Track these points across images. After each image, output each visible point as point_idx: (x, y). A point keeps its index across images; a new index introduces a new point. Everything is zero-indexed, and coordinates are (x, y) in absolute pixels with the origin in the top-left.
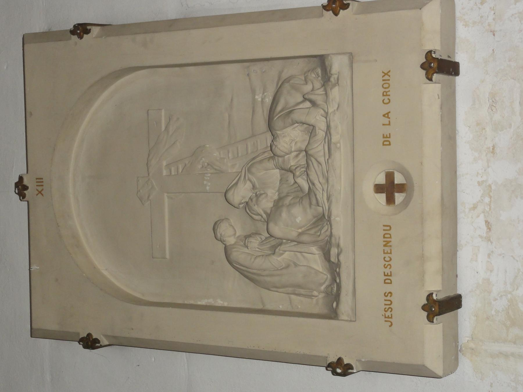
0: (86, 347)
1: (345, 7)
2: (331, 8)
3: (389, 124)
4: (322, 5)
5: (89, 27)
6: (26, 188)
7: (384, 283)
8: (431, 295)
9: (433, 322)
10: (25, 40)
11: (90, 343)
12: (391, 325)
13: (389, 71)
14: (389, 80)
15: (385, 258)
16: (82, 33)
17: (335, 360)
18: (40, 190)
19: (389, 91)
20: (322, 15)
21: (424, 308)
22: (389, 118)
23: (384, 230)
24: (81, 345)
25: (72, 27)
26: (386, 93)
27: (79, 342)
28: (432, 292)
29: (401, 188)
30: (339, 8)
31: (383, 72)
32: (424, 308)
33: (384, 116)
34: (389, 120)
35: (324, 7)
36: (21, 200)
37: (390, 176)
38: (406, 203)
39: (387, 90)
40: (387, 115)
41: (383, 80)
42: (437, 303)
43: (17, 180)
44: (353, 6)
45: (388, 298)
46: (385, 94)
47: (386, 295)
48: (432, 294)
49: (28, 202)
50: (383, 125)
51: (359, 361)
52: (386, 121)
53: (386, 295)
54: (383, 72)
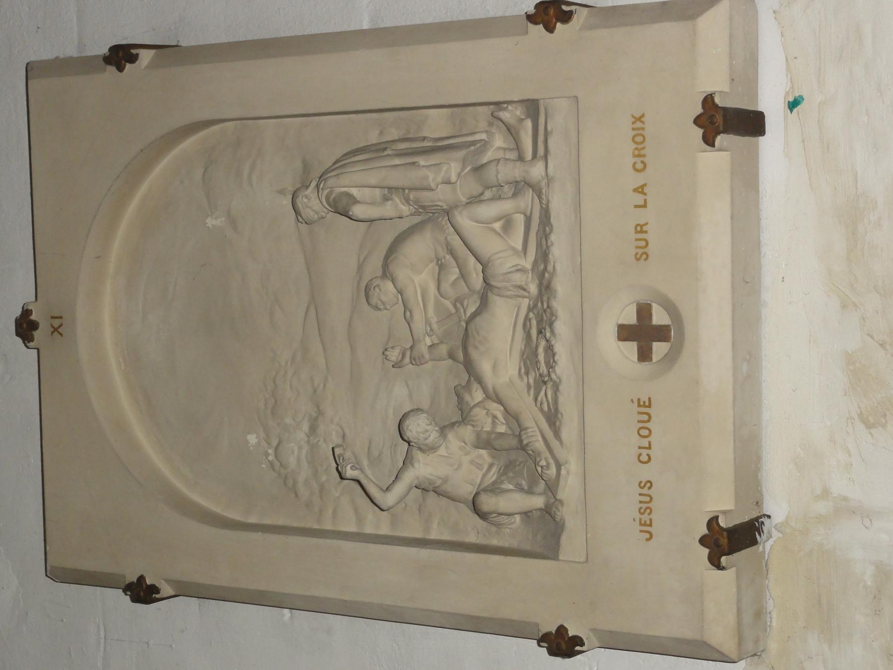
0: (136, 599)
1: (566, 17)
2: (540, 20)
3: (645, 206)
4: (526, 13)
5: (134, 51)
6: (34, 326)
7: (636, 233)
8: (715, 519)
9: (713, 145)
10: (30, 70)
11: (142, 594)
12: (647, 420)
13: (643, 115)
14: (643, 129)
15: (640, 455)
16: (123, 62)
17: (553, 629)
18: (56, 326)
19: (644, 148)
20: (526, 32)
21: (697, 121)
22: (645, 194)
23: (639, 422)
24: (128, 596)
25: (107, 51)
26: (642, 228)
27: (125, 591)
28: (787, 103)
29: (662, 333)
30: (556, 19)
31: (633, 116)
32: (697, 121)
33: (635, 190)
34: (645, 197)
35: (531, 18)
36: (28, 348)
37: (644, 311)
38: (671, 358)
39: (640, 146)
40: (640, 190)
41: (633, 129)
42: (725, 534)
43: (18, 312)
44: (580, 17)
45: (645, 491)
46: (639, 229)
47: (642, 485)
48: (717, 518)
49: (38, 349)
50: (636, 206)
51: (594, 630)
52: (639, 199)
53: (642, 485)
54: (633, 116)
